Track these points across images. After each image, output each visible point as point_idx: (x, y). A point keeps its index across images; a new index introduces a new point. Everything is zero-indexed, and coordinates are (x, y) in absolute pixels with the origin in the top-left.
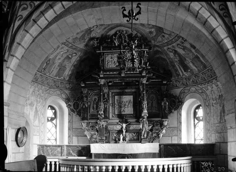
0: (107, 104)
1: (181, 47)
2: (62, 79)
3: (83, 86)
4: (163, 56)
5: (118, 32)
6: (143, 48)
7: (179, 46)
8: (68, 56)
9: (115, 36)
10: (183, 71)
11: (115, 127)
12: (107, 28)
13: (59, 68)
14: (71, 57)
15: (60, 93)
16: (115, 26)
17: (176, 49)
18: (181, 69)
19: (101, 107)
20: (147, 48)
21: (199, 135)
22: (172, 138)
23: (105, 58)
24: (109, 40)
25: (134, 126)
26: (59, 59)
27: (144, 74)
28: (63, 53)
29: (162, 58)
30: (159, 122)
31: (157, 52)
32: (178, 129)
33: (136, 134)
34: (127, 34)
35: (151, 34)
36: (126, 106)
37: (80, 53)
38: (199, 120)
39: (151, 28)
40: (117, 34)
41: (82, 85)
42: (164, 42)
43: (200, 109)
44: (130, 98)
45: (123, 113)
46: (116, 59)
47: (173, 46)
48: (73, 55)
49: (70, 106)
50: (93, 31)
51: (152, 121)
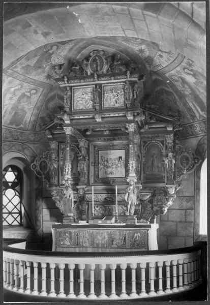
0: (84, 164)
1: (190, 72)
2: (21, 128)
3: (171, 131)
4: (166, 89)
5: (91, 54)
6: (128, 77)
7: (186, 70)
8: (24, 93)
9: (88, 60)
10: (199, 110)
12: (75, 48)
13: (14, 112)
14: (29, 96)
15: (20, 148)
16: (85, 43)
17: (183, 76)
18: (197, 110)
20: (135, 76)
21: (8, 201)
23: (74, 94)
24: (77, 68)
26: (11, 99)
27: (130, 118)
28: (15, 90)
29: (167, 92)
30: (163, 189)
34: (105, 57)
37: (41, 89)
39: (141, 44)
40: (90, 56)
41: (49, 137)
42: (164, 66)
43: (13, 172)
44: (122, 153)
45: (110, 176)
46: (88, 97)
47: (178, 72)
49: (35, 168)
50: (53, 53)
51: (152, 187)
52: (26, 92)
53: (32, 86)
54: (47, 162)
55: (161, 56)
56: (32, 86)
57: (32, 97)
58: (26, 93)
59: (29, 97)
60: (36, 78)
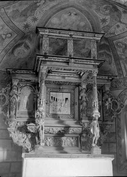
11: (51, 129)
14: (4, 38)
19: (42, 101)
22: (109, 145)
25: (74, 130)
31: (36, 47)
32: (117, 135)
33: (74, 139)
35: (27, 25)
36: (62, 104)
37: (16, 35)
38: (32, 133)
42: (116, 34)
48: (7, 36)
52: (4, 34)
53: (11, 31)
54: (6, 96)
55: (118, 26)
56: (11, 31)
57: (6, 40)
58: (2, 35)
59: (3, 39)
60: (17, 24)
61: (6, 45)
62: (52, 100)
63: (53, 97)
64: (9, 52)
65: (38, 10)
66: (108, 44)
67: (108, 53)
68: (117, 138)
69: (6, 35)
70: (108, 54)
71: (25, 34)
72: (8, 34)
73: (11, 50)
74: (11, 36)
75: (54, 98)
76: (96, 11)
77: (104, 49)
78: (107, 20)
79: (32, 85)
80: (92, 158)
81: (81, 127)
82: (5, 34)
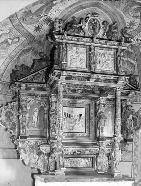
61: (12, 51)
62: (65, 116)
63: (69, 114)
64: (14, 59)
65: (53, 10)
66: (132, 51)
67: (132, 61)
68: (133, 157)
69: (12, 39)
70: (131, 64)
71: (35, 38)
72: (16, 39)
73: (17, 57)
74: (19, 40)
75: (67, 114)
76: (123, 13)
77: (127, 57)
78: (135, 23)
79: (41, 99)
80: (112, 181)
81: (98, 148)
82: (12, 38)
